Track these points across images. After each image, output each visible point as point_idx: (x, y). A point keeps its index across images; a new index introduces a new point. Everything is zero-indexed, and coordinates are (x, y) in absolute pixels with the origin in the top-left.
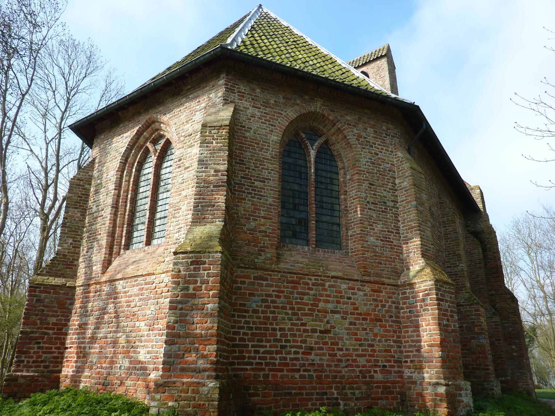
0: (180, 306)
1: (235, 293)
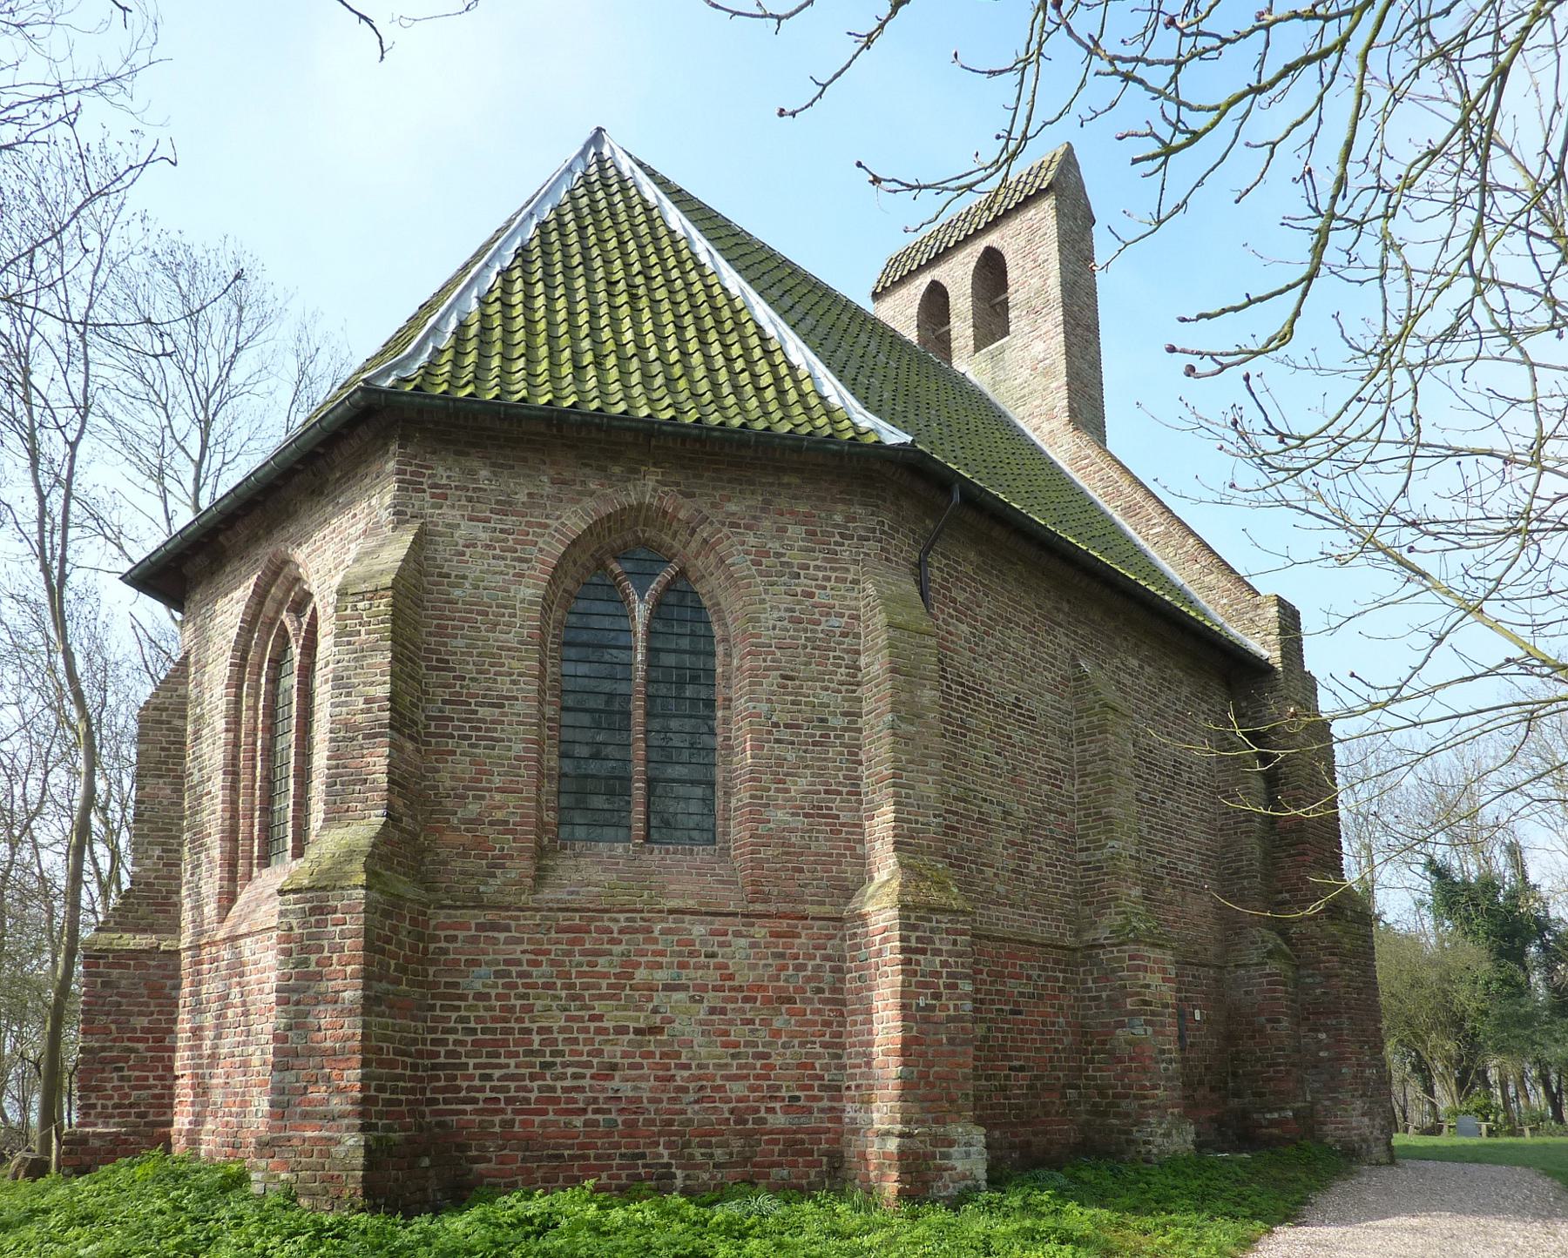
0: (295, 997)
1: (434, 962)
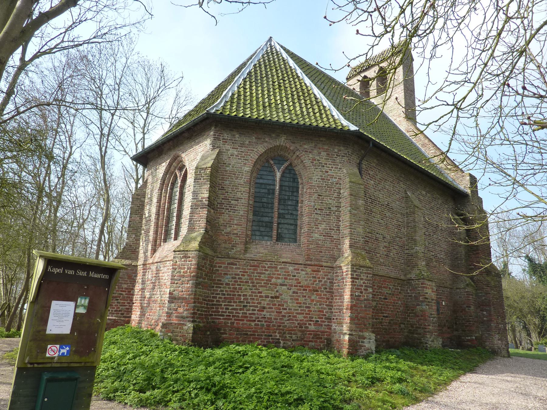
0: (176, 282)
1: (215, 273)
